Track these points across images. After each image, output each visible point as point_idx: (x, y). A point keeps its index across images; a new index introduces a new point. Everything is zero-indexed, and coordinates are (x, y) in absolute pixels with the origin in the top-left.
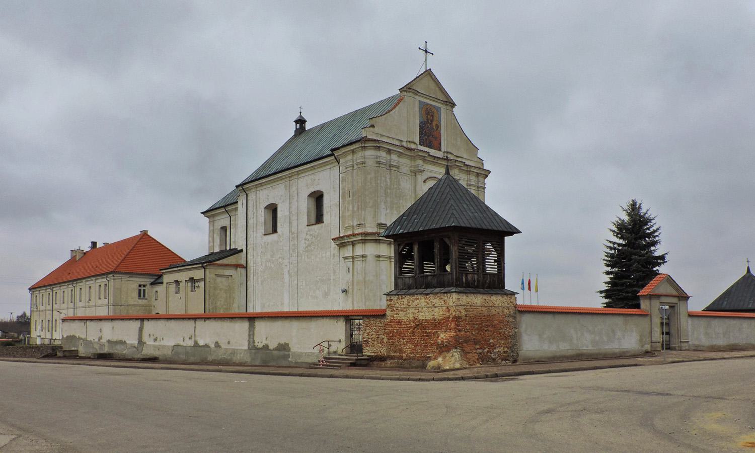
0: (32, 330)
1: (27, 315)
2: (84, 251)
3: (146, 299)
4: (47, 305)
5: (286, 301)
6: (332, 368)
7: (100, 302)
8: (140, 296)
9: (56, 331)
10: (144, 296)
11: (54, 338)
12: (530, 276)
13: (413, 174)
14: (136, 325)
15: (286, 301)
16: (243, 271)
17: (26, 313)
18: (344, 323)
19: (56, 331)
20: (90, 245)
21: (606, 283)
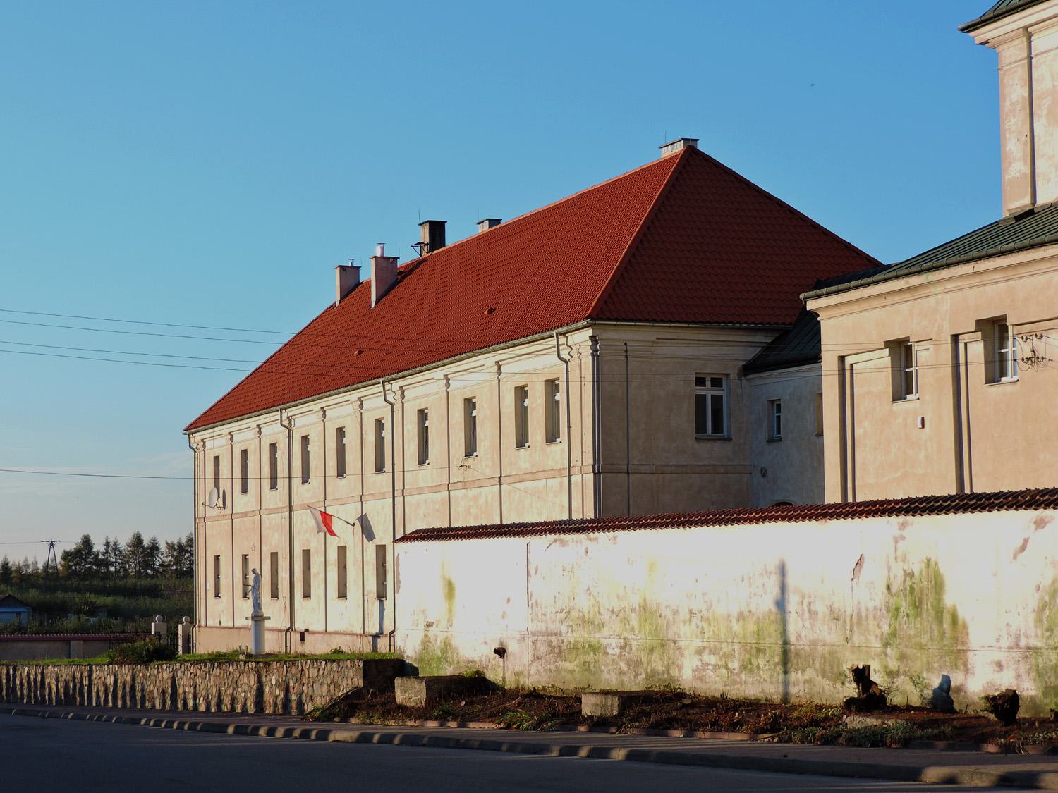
0: (200, 592)
1: (95, 549)
2: (400, 263)
3: (729, 439)
4: (297, 481)
5: (472, 521)
6: (972, 28)
7: (522, 460)
8: (700, 427)
9: (307, 595)
10: (717, 427)
11: (300, 626)
12: (220, 618)
13: (923, 647)
14: (236, 625)
15: (472, 521)
16: (854, 365)
17: (93, 540)
18: (1038, 702)
19: (307, 595)
20: (424, 235)
21: (19, 564)
